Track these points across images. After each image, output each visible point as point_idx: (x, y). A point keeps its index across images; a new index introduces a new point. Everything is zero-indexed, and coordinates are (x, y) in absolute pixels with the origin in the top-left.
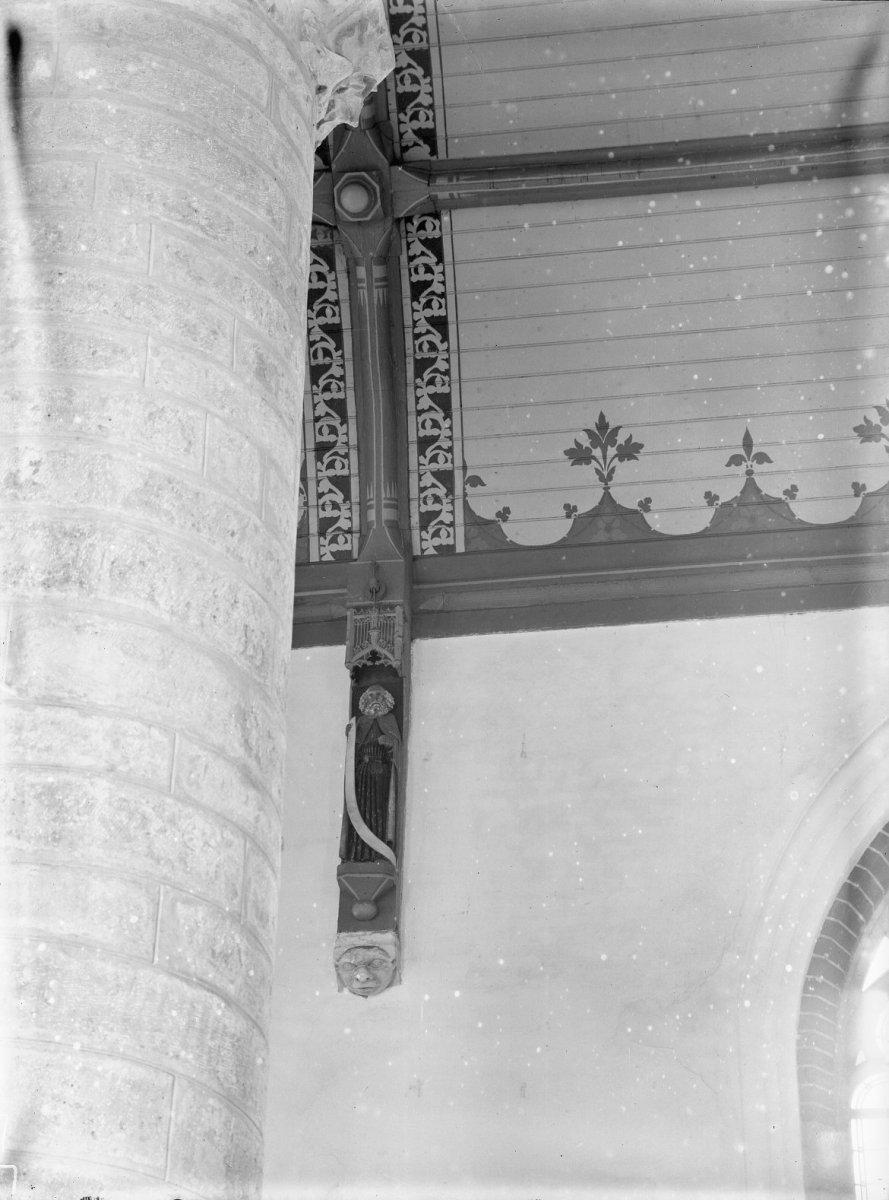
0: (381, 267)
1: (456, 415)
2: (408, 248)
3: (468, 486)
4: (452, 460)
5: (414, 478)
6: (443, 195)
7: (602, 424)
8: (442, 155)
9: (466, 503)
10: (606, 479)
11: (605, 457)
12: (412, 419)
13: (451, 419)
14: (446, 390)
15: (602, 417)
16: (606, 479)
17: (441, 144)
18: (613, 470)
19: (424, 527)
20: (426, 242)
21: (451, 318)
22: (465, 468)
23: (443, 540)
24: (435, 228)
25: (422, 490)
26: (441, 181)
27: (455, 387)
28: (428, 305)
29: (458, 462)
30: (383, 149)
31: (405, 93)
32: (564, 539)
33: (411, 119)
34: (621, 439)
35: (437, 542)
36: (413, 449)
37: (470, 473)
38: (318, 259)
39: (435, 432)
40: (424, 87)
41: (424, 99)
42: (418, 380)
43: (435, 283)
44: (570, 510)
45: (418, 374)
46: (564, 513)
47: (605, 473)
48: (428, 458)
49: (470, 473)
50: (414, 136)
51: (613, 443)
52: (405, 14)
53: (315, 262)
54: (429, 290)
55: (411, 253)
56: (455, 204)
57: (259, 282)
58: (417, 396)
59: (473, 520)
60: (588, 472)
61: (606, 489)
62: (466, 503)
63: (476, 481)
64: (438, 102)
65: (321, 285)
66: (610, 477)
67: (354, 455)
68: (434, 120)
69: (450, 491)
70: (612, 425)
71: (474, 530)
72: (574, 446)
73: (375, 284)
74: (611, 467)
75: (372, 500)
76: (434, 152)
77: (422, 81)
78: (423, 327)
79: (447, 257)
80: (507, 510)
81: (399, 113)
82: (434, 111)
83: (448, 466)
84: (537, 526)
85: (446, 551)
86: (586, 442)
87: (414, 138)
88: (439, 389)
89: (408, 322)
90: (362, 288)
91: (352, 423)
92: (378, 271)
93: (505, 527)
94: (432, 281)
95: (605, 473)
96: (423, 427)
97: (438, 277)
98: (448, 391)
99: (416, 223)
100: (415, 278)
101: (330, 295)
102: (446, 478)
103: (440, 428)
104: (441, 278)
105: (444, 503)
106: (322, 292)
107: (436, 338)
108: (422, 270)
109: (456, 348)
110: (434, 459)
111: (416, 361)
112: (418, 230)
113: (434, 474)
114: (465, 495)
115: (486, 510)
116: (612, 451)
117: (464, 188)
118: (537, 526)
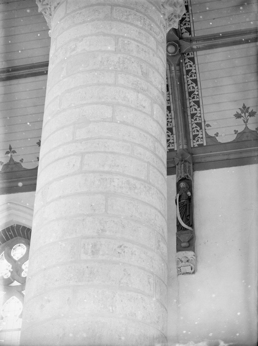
0: (178, 67)
1: (201, 107)
2: (190, 104)
3: (206, 127)
4: (201, 119)
5: (190, 125)
6: (195, 47)
7: (244, 107)
8: (193, 36)
9: (206, 132)
10: (246, 122)
11: (245, 116)
12: (189, 109)
13: (189, 13)
14: (198, 99)
15: (244, 105)
16: (246, 122)
17: (192, 33)
18: (248, 120)
19: (194, 139)
20: (197, 124)
21: (198, 80)
22: (205, 122)
23: (200, 142)
24: (192, 54)
25: (193, 128)
26: (194, 43)
27: (192, 24)
28: (198, 141)
29: (203, 120)
30: (178, 36)
31: (190, 91)
32: (234, 140)
33: (190, 77)
34: (250, 111)
35: (198, 143)
36: (190, 117)
37: (206, 123)
38: (168, 131)
39: (196, 112)
40: (194, 68)
41: (194, 71)
42: (190, 98)
43: (193, 70)
44: (236, 132)
45: (190, 96)
46: (234, 133)
47: (246, 121)
48: (196, 141)
49: (206, 123)
50: (191, 81)
51: (247, 112)
52: (190, 69)
53: (167, 132)
54: (185, 20)
55: (193, 127)
56: (199, 49)
57: (135, 24)
58: (190, 102)
59: (208, 137)
60: (241, 120)
61: (246, 125)
62: (206, 132)
63: (208, 125)
64: (197, 72)
65: (169, 138)
66: (247, 122)
67: (175, 144)
68: (203, 141)
69: (201, 128)
70: (247, 107)
71: (209, 140)
72: (236, 113)
73: (177, 72)
74: (247, 118)
75: (180, 143)
76: (190, 34)
77: (193, 66)
78: (190, 82)
79: (196, 62)
80: (217, 133)
81: (187, 75)
82: (196, 74)
83: (200, 121)
84: (226, 136)
85: (201, 145)
86: (240, 112)
87: (191, 82)
88: (196, 100)
89: (186, 81)
90: (173, 73)
91: (172, 112)
92: (178, 68)
93: (217, 138)
94: (186, 17)
95: (246, 121)
96: (190, 89)
97: (196, 90)
98: (196, 78)
99: (187, 54)
100: (187, 69)
101: (171, 141)
102: (199, 125)
103: (197, 110)
104: (195, 68)
105: (200, 131)
106: (169, 140)
107: (194, 85)
108: (189, 66)
109: (192, 22)
110: (196, 120)
111: (188, 92)
112: (187, 55)
113: (194, 102)
114: (205, 130)
115: (211, 133)
116: (247, 114)
117: (201, 44)
118: (226, 136)
